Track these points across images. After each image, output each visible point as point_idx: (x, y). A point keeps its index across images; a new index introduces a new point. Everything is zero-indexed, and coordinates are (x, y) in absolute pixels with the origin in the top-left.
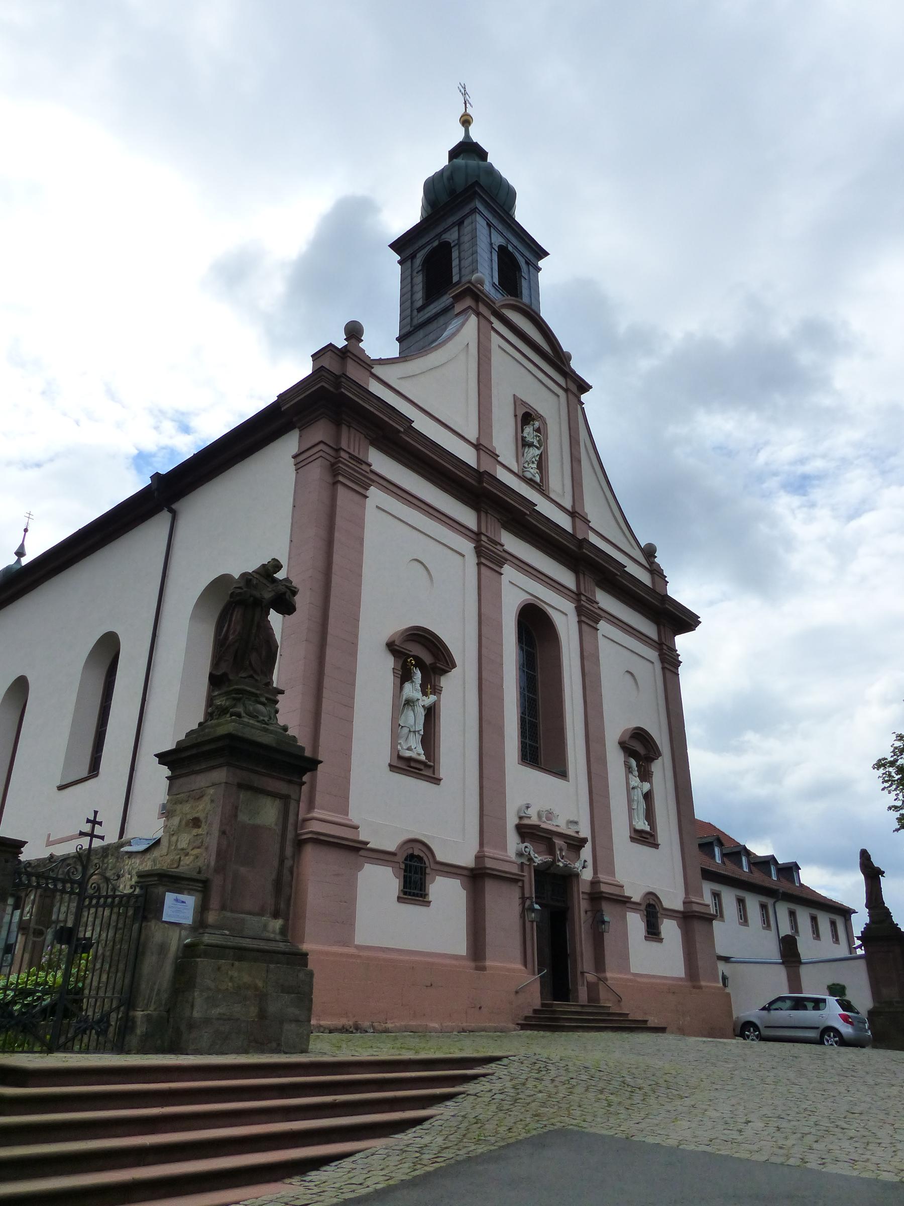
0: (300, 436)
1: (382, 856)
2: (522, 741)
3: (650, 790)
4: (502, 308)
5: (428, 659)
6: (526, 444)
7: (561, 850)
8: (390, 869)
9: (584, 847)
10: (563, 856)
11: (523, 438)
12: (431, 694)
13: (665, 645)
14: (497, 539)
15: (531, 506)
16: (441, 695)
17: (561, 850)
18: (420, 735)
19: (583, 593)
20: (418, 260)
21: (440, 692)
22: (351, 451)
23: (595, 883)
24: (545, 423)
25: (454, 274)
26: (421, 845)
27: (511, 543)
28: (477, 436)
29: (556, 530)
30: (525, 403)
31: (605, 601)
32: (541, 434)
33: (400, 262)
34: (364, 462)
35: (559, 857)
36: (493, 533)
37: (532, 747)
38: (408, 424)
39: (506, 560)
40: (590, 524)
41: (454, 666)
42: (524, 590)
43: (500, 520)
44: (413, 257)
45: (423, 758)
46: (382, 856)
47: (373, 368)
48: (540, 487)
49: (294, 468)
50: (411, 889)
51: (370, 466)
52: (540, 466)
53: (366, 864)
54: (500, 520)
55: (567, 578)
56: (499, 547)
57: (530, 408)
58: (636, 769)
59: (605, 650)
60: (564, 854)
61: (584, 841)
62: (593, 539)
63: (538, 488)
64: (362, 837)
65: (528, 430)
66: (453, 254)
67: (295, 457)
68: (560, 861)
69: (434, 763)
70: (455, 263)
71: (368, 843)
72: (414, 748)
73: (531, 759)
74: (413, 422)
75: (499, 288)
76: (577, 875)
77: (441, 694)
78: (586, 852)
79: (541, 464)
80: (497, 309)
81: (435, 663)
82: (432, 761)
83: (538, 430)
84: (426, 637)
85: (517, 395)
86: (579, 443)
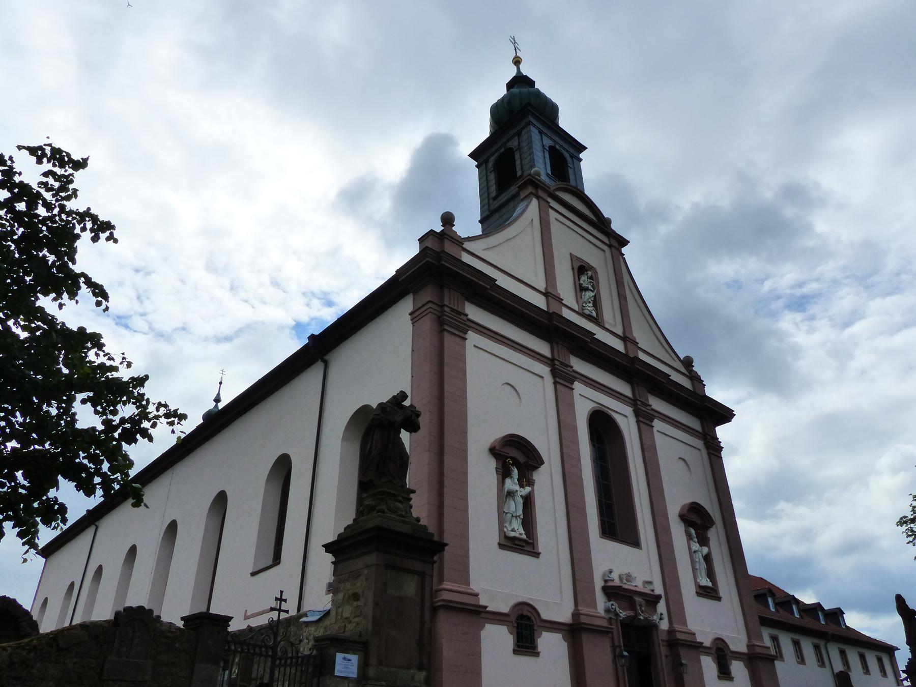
0: (414, 299)
1: (498, 618)
5: (522, 459)
6: (583, 289)
11: (580, 285)
13: (640, 401)
14: (567, 363)
17: (641, 606)
20: (490, 164)
23: (671, 632)
24: (595, 272)
28: (545, 287)
44: (486, 161)
45: (524, 537)
46: (498, 618)
48: (597, 320)
58: (695, 536)
60: (643, 609)
65: (584, 278)
66: (516, 157)
67: (411, 314)
70: (518, 162)
71: (487, 607)
72: (517, 529)
76: (656, 626)
78: (662, 607)
83: (591, 278)
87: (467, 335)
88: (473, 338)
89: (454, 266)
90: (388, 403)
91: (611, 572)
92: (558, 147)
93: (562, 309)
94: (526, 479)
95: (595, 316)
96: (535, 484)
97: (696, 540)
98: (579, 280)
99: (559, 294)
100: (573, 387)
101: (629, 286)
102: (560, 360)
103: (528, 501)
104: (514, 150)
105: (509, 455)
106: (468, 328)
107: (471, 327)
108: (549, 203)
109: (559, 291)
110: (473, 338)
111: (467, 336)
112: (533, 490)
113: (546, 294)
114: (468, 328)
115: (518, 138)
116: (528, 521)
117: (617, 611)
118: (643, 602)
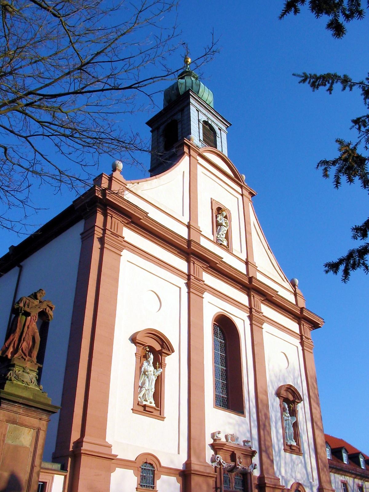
0: (85, 223)
1: (126, 464)
2: (216, 395)
3: (296, 421)
4: (204, 152)
5: (158, 347)
6: (219, 225)
7: (239, 458)
8: (132, 471)
9: (254, 456)
10: (241, 462)
11: (217, 221)
12: (159, 368)
13: (304, 336)
14: (200, 278)
15: (220, 259)
16: (165, 368)
17: (239, 458)
18: (152, 392)
19: (304, 335)
20: (161, 130)
21: (165, 365)
22: (112, 230)
23: (261, 478)
24: (229, 211)
25: (179, 136)
26: (153, 457)
27: (209, 279)
28: (188, 221)
29: (230, 269)
30: (218, 202)
31: (267, 311)
32: (227, 219)
33: (151, 131)
34: (201, 280)
35: (238, 462)
36: (198, 275)
37: (224, 398)
38: (146, 215)
39: (206, 290)
40: (258, 269)
41: (173, 351)
42: (219, 308)
43: (202, 267)
44: (158, 128)
45: (153, 405)
46: (126, 464)
47: (127, 185)
48: (228, 248)
49: (81, 240)
50: (150, 484)
51: (124, 238)
52: (227, 238)
53: (116, 468)
54: (202, 267)
55: (243, 298)
56: (201, 282)
57: (220, 204)
58: (288, 409)
59: (266, 338)
60: (241, 461)
61: (254, 453)
62: (260, 277)
63: (226, 249)
64: (113, 453)
65: (220, 217)
66: (178, 126)
67: (81, 234)
68: (239, 465)
69: (160, 408)
70: (179, 130)
71: (117, 456)
72: (150, 402)
73: (223, 404)
74: (148, 213)
75: (203, 142)
76: (251, 474)
77: (165, 367)
78: (256, 460)
79: (227, 237)
80: (201, 153)
81: (162, 350)
82: (159, 407)
83: (226, 217)
84: (162, 338)
85: (214, 198)
86: (250, 223)
87: (122, 253)
88: (126, 254)
89: (128, 207)
90: (170, 354)
91: (219, 433)
92: (210, 122)
93: (200, 237)
94: (158, 363)
95: (226, 245)
96: (166, 367)
97: (288, 412)
98: (216, 218)
99: (199, 227)
100: (121, 254)
101: (254, 225)
102: (305, 335)
103: (159, 381)
104: (178, 121)
105: (147, 345)
106: (124, 248)
107: (125, 247)
108: (198, 160)
109: (199, 225)
110: (126, 254)
111: (263, 326)
112: (164, 371)
113: (189, 226)
114: (124, 248)
115: (182, 114)
116: (158, 396)
117: (222, 462)
118: (242, 456)
